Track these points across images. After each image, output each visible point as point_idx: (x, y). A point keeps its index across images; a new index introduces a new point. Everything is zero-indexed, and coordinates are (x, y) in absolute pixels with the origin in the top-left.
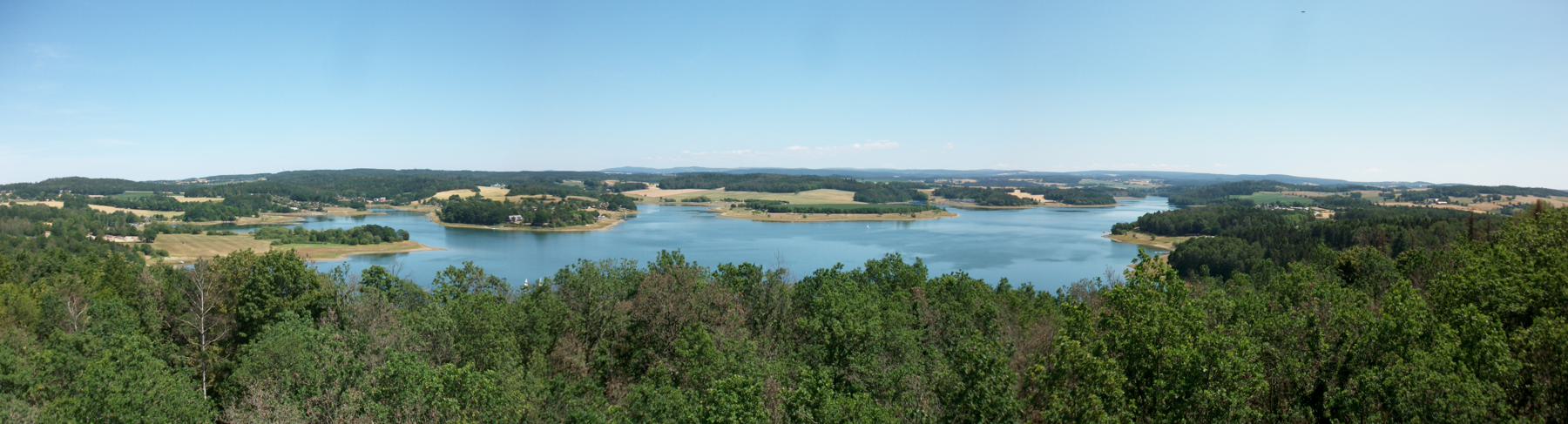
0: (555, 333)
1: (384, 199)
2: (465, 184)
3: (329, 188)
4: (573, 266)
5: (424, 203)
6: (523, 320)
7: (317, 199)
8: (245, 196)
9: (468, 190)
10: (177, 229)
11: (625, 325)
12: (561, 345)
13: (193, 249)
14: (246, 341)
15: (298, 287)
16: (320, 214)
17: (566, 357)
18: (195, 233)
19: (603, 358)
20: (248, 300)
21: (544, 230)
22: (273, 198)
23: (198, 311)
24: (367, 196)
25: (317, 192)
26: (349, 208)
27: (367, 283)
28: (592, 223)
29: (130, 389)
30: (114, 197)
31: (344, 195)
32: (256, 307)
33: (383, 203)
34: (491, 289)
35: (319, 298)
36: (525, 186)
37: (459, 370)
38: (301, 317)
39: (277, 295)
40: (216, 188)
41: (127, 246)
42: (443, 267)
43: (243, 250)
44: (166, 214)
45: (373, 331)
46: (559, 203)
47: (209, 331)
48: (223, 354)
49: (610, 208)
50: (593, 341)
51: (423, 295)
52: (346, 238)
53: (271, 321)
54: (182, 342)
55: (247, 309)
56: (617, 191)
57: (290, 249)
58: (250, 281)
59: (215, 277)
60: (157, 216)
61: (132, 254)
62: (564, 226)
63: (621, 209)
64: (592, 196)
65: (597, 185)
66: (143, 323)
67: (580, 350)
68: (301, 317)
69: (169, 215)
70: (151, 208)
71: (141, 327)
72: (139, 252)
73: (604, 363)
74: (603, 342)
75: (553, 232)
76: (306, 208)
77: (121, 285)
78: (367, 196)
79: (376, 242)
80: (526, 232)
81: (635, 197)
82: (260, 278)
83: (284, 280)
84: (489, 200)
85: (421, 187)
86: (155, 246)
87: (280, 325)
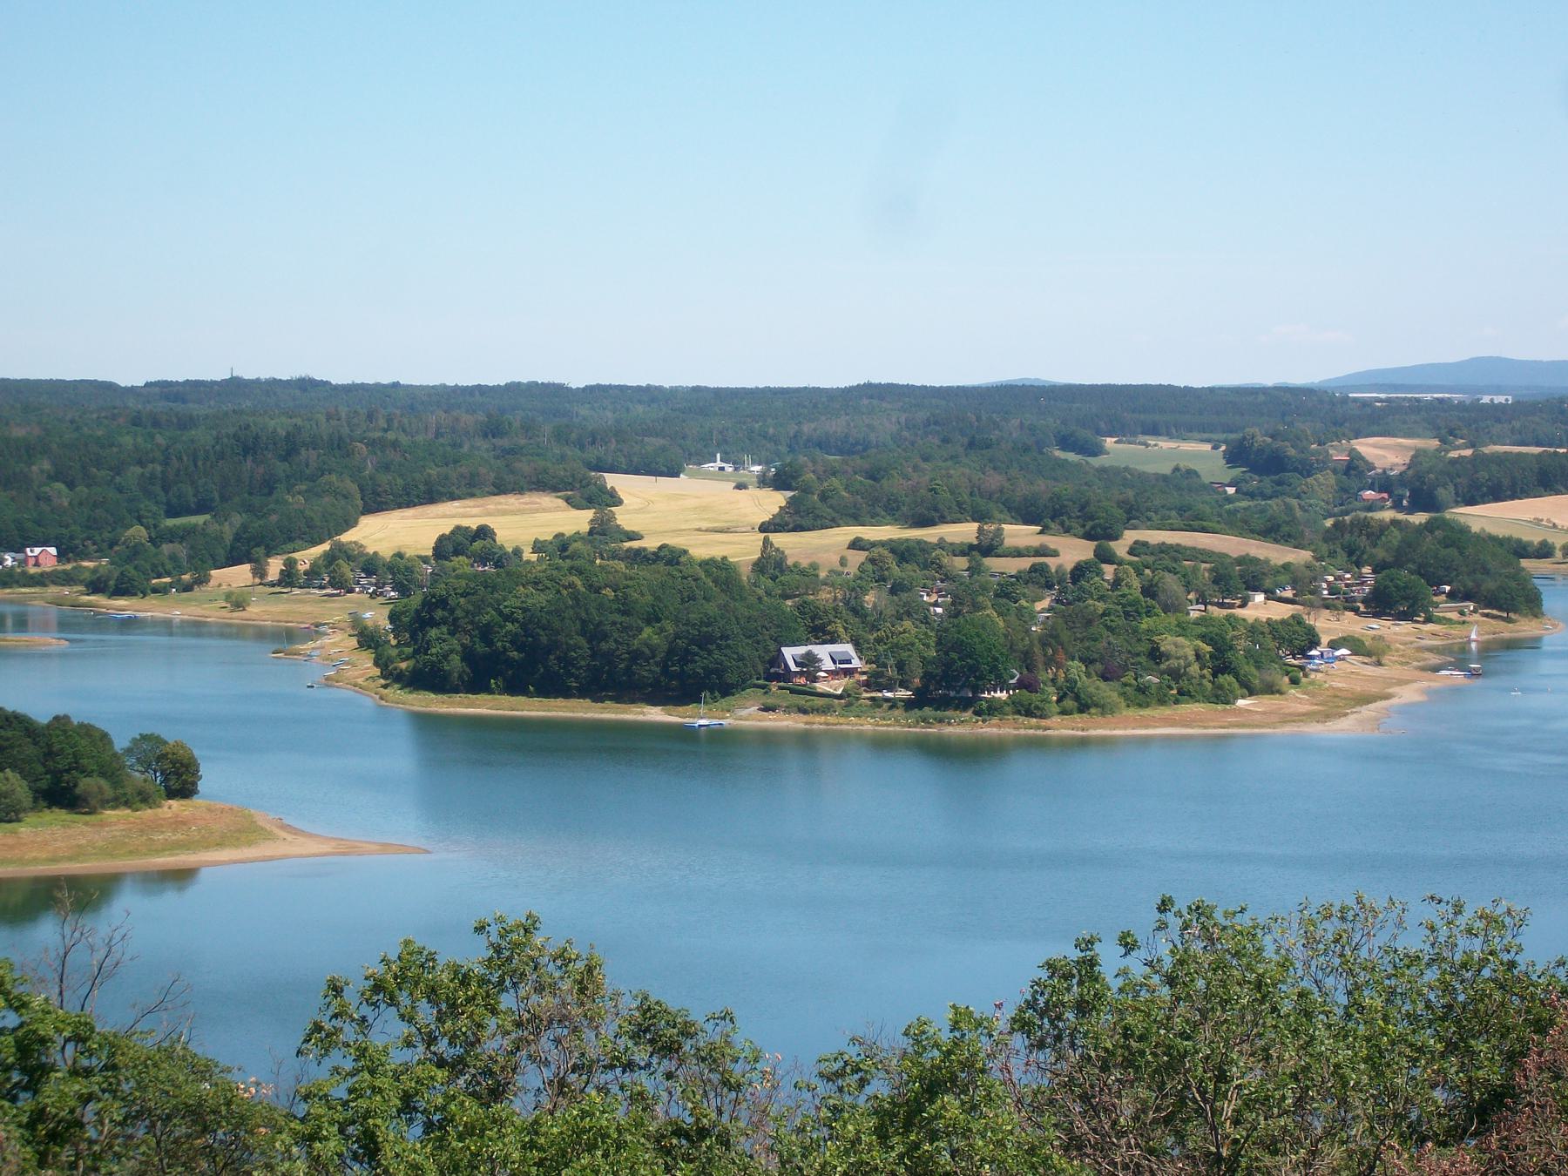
1: (45, 556)
4: (1128, 944)
5: (288, 578)
9: (547, 500)
21: (990, 729)
28: (1271, 689)
33: (40, 580)
36: (873, 476)
46: (1080, 572)
49: (1381, 604)
51: (242, 1121)
56: (1423, 499)
62: (1105, 709)
63: (1447, 609)
64: (1272, 532)
65: (1306, 470)
75: (1037, 745)
80: (881, 745)
81: (1534, 537)
84: (670, 557)
85: (268, 486)
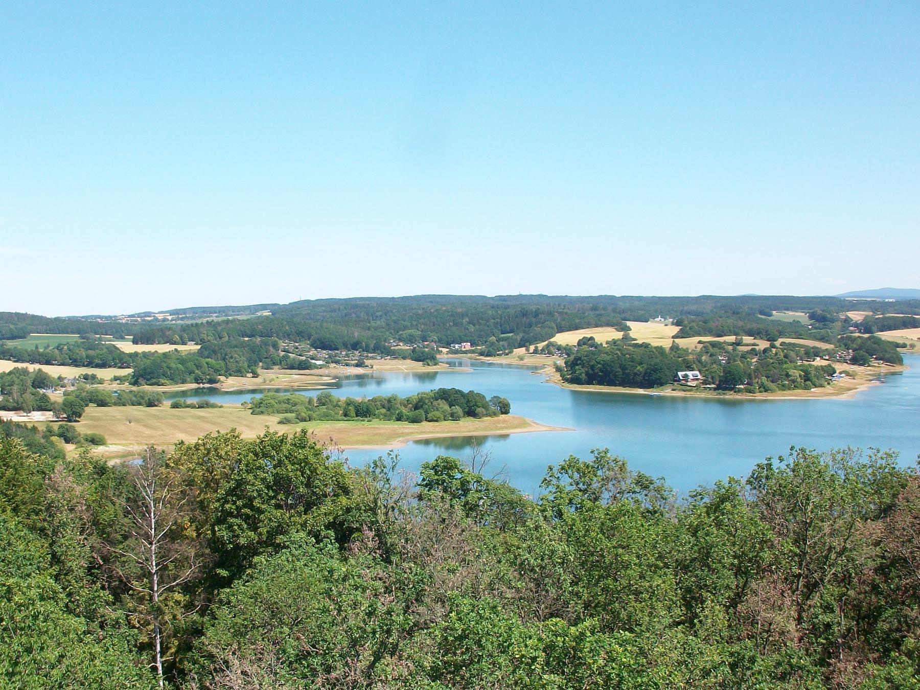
0: (746, 573)
1: (467, 346)
2: (603, 319)
3: (376, 329)
4: (781, 459)
5: (536, 351)
6: (686, 549)
7: (355, 346)
8: (234, 343)
9: (610, 329)
10: (119, 398)
11: (871, 564)
12: (755, 592)
13: (147, 432)
14: (227, 582)
15: (314, 493)
16: (360, 371)
17: (763, 614)
18: (151, 404)
19: (827, 618)
20: (231, 514)
21: (738, 397)
22: (282, 344)
23: (147, 537)
24: (440, 341)
25: (356, 334)
26: (409, 361)
27: (430, 485)
28: (821, 386)
29: (20, 668)
30: (11, 344)
31: (400, 340)
32: (245, 526)
33: (465, 352)
34: (639, 497)
35: (348, 510)
37: (573, 629)
38: (318, 542)
39: (278, 507)
40: (185, 329)
41: (34, 429)
42: (558, 460)
43: (223, 432)
44: (101, 373)
45: (436, 568)
46: (765, 351)
47: (165, 568)
48: (189, 606)
49: (855, 361)
50: (812, 587)
52: (404, 411)
53: (270, 549)
54: (120, 590)
55: (230, 527)
56: (868, 330)
57: (299, 430)
58: (233, 484)
59: (176, 478)
60: (86, 377)
61: (43, 441)
62: (772, 391)
63: (874, 363)
64: (822, 339)
65: (833, 321)
66: (56, 559)
67: (788, 602)
68: (318, 542)
69: (106, 374)
70: (75, 363)
71: (51, 565)
72: (54, 439)
73: (828, 626)
74: (829, 591)
76: (337, 362)
77: (16, 495)
78: (440, 341)
79: (454, 417)
80: (707, 401)
81: (901, 342)
82: (250, 477)
83: (289, 480)
84: (646, 346)
86: (82, 427)
87: (284, 555)
